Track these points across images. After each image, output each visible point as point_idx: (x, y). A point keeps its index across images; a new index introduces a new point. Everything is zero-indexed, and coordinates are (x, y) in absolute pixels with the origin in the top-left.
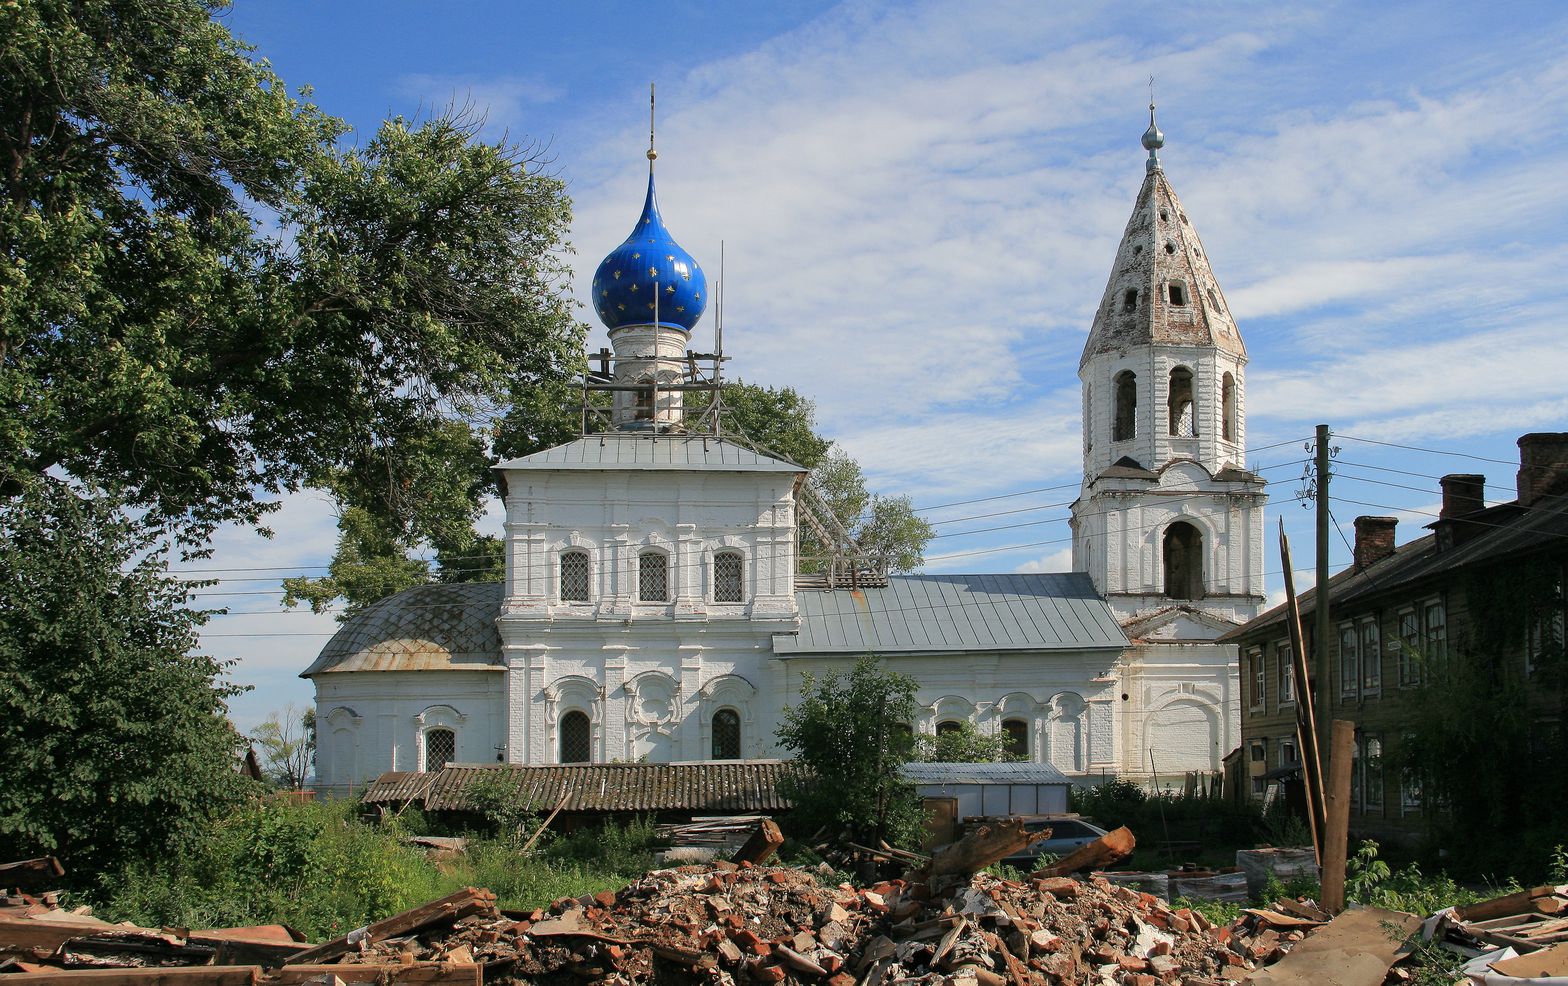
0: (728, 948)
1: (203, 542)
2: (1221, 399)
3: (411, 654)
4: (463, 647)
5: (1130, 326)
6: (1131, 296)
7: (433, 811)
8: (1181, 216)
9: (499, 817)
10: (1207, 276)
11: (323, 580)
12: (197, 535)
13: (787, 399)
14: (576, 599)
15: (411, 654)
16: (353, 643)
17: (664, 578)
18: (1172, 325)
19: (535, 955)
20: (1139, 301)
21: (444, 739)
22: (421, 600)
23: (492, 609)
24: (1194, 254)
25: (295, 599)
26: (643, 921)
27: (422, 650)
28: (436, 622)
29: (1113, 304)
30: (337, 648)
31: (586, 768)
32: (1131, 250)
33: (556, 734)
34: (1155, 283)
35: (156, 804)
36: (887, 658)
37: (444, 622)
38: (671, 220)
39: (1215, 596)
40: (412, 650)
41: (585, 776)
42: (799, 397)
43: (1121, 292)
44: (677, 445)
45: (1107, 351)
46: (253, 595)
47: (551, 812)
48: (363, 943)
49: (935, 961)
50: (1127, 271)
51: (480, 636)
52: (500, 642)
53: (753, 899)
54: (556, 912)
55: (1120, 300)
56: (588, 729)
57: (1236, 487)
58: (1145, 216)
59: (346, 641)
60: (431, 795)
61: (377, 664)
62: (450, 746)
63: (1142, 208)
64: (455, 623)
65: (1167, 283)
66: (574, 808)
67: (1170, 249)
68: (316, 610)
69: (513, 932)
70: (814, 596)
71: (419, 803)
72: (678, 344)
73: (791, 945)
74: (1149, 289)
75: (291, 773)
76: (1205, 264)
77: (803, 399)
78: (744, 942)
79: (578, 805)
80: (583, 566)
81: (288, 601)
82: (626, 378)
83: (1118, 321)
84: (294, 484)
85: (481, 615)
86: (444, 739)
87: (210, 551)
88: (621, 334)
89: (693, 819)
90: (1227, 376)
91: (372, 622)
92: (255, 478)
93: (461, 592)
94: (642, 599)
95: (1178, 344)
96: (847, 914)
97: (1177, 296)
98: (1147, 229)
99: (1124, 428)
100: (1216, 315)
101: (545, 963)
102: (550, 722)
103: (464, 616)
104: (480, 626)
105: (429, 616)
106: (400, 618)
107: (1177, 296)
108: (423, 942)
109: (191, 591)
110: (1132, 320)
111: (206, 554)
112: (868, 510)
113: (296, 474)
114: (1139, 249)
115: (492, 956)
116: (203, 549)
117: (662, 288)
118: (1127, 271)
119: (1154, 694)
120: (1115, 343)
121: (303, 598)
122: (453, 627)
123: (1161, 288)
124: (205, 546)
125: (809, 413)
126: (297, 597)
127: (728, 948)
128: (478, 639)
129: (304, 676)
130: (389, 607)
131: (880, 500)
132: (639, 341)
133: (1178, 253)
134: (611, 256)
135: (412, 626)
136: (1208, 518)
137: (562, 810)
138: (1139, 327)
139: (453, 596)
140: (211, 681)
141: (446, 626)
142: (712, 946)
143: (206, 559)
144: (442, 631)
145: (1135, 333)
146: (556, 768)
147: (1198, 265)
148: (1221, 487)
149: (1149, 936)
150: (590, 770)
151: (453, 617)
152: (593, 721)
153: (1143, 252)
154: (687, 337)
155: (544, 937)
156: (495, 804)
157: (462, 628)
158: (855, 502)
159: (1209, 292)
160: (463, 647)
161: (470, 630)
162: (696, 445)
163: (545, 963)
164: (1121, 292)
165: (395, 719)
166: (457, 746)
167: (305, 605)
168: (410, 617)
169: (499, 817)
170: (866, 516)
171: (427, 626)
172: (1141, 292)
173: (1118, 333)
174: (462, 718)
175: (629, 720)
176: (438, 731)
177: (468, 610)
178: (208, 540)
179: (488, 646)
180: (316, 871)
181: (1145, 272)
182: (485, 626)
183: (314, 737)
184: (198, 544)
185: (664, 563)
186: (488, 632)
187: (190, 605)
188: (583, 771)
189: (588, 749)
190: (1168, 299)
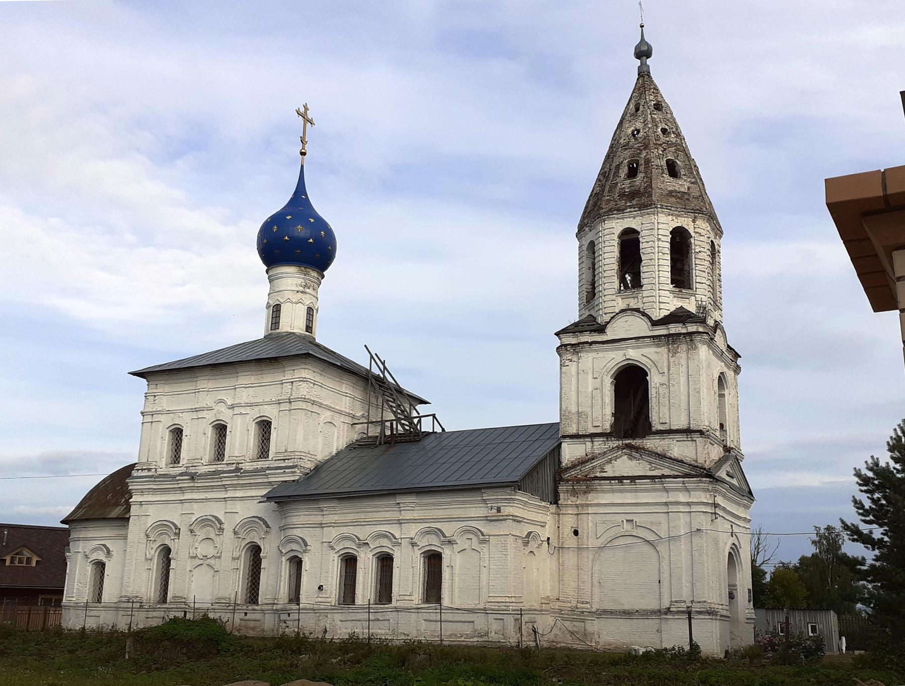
18: (622, 195)
148: (661, 331)
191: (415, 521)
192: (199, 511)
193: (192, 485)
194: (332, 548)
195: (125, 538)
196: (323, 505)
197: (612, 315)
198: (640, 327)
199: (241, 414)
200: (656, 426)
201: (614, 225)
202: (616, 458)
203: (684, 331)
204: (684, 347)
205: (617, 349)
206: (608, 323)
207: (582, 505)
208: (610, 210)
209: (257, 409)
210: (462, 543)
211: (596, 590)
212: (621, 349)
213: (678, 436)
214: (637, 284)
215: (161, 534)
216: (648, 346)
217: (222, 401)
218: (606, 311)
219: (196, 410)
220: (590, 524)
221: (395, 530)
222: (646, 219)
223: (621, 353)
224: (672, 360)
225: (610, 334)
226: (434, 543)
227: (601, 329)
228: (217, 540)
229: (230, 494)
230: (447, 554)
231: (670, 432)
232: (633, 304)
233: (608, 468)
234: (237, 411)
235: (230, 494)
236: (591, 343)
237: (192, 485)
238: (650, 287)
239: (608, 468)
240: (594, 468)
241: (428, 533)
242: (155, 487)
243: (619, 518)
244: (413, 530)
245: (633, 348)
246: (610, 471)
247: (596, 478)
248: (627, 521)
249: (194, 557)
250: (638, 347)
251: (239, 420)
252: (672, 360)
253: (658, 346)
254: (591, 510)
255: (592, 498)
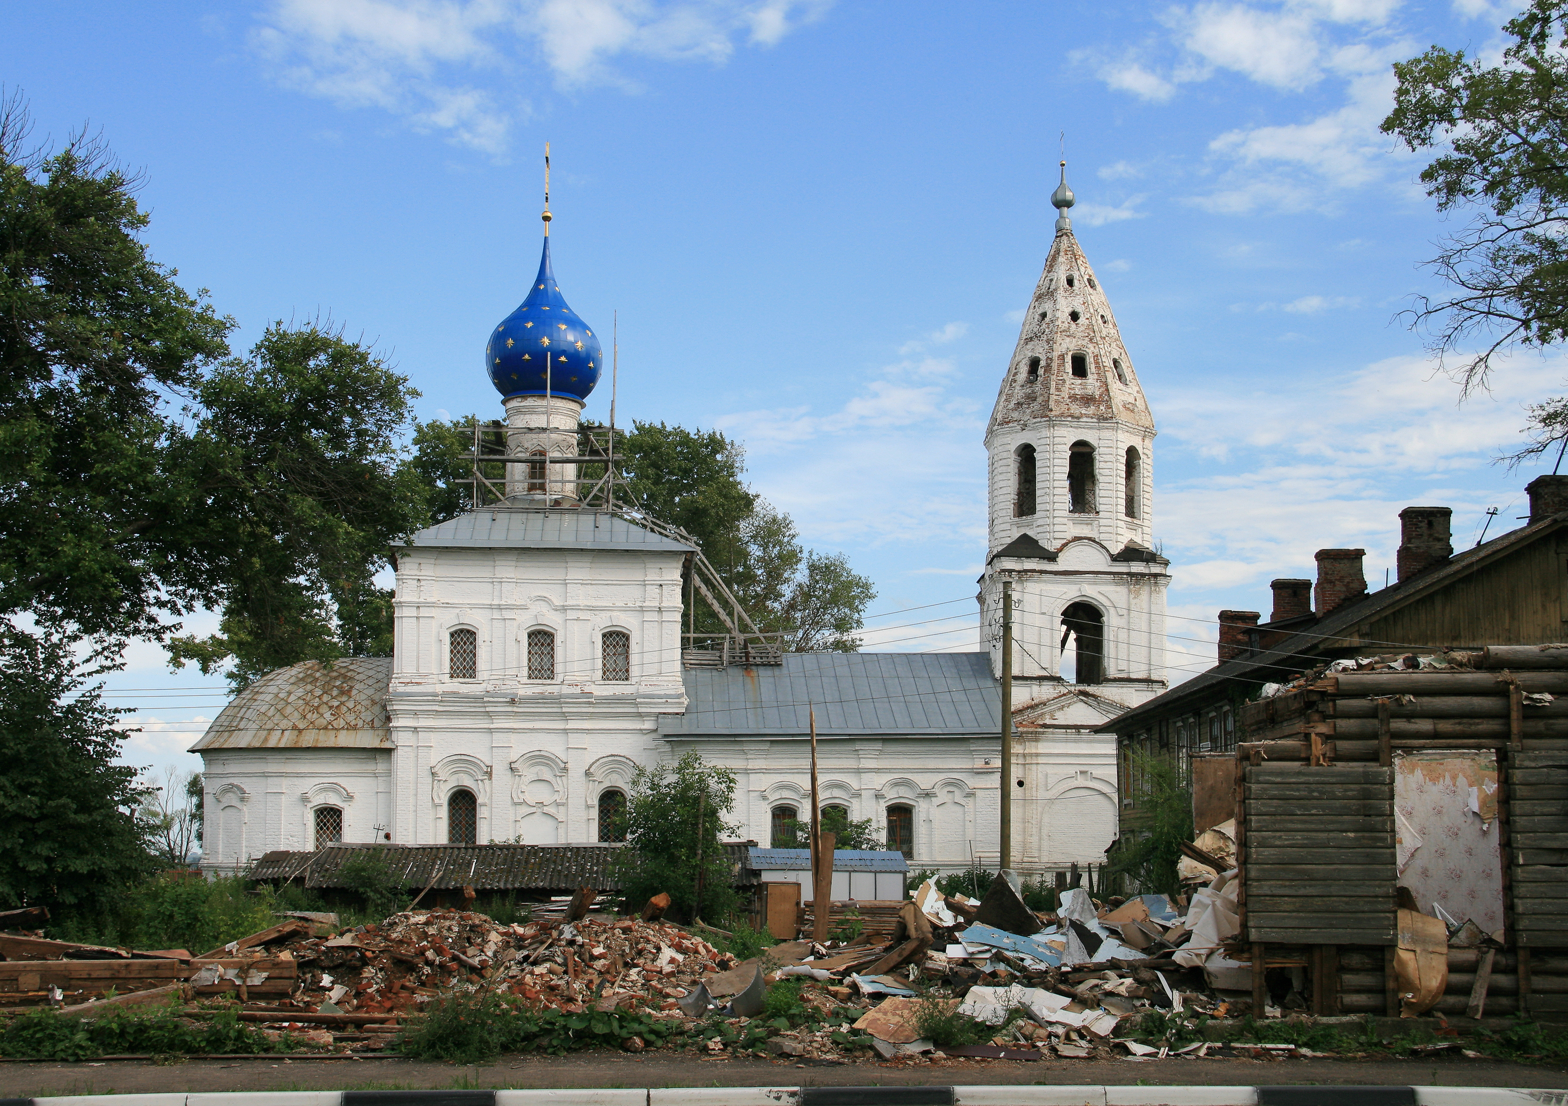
0: (430, 954)
1: (117, 657)
2: (1123, 475)
3: (300, 731)
4: (352, 724)
5: (1031, 398)
6: (1034, 364)
7: (313, 888)
8: (1089, 281)
9: (371, 894)
10: (1114, 345)
11: (213, 637)
12: (112, 652)
13: (716, 444)
14: (464, 676)
15: (300, 731)
16: (242, 718)
17: (552, 657)
18: (1073, 398)
19: (327, 957)
20: (1041, 371)
21: (332, 817)
22: (311, 675)
23: (380, 685)
24: (1100, 321)
25: (182, 659)
26: (386, 938)
27: (311, 726)
28: (325, 698)
29: (1016, 374)
30: (226, 724)
31: (459, 849)
32: (1037, 317)
33: (444, 812)
34: (1055, 354)
35: (91, 874)
36: (772, 742)
37: (333, 698)
38: (566, 285)
39: (1115, 680)
40: (301, 726)
41: (457, 856)
42: (727, 441)
43: (1024, 362)
44: (568, 520)
45: (1007, 423)
46: (156, 698)
47: (422, 890)
48: (234, 950)
49: (531, 959)
50: (1031, 339)
51: (369, 713)
52: (388, 719)
53: (450, 929)
54: (342, 934)
55: (1024, 369)
56: (475, 809)
57: (1137, 567)
58: (1051, 280)
59: (236, 716)
60: (311, 873)
61: (266, 740)
62: (338, 824)
63: (1049, 272)
64: (344, 699)
65: (1070, 354)
66: (443, 887)
67: (1075, 316)
68: (205, 670)
69: (317, 945)
70: (705, 676)
71: (299, 881)
72: (573, 413)
73: (464, 953)
74: (1051, 359)
75: (171, 850)
76: (1112, 331)
77: (732, 444)
78: (439, 951)
79: (448, 883)
80: (471, 643)
81: (176, 662)
82: (519, 449)
83: (1019, 393)
84: (192, 605)
85: (370, 692)
86: (332, 817)
87: (124, 665)
88: (514, 403)
89: (553, 898)
90: (1132, 453)
91: (261, 697)
92: (161, 604)
93: (351, 667)
94: (530, 677)
95: (1078, 418)
96: (500, 938)
97: (1079, 367)
98: (1052, 295)
99: (1026, 503)
100: (1121, 386)
101: (332, 961)
102: (437, 801)
103: (354, 692)
104: (369, 702)
105: (318, 692)
106: (290, 693)
107: (1079, 367)
108: (267, 950)
109: (117, 716)
110: (1033, 392)
111: (120, 667)
112: (802, 567)
113: (192, 597)
114: (1044, 315)
115: (304, 957)
116: (117, 663)
117: (555, 356)
118: (1031, 339)
119: (1051, 781)
120: (1015, 415)
121: (192, 657)
122: (342, 703)
123: (1062, 357)
124: (118, 660)
125: (738, 459)
126: (185, 657)
127: (430, 954)
128: (367, 716)
129: (193, 751)
130: (279, 682)
131: (815, 557)
132: (532, 411)
133: (1082, 320)
134: (504, 323)
135: (301, 702)
136: (1107, 595)
137: (432, 889)
138: (1040, 400)
139: (343, 671)
140: (130, 782)
141: (336, 703)
142: (422, 952)
143: (120, 671)
144: (331, 707)
145: (1036, 406)
146: (445, 848)
147: (1104, 334)
148: (1122, 568)
149: (668, 953)
150: (463, 850)
151: (342, 693)
152: (479, 801)
153: (1047, 320)
154: (583, 406)
155: (333, 947)
156: (369, 883)
157: (351, 705)
158: (790, 558)
159: (1115, 362)
160: (352, 724)
161: (359, 707)
162: (587, 520)
163: (332, 961)
164: (1024, 362)
165: (283, 796)
166: (345, 825)
167: (192, 665)
168: (300, 692)
169: (371, 894)
170: (801, 575)
171: (316, 702)
172: (1043, 363)
173: (1019, 404)
174: (350, 797)
175: (516, 800)
176: (325, 809)
177: (357, 687)
178: (121, 656)
179: (377, 723)
180: (207, 927)
181: (1048, 341)
182: (374, 703)
183: (200, 806)
184: (113, 660)
185: (553, 641)
186: (377, 709)
187: (117, 727)
188: (456, 852)
189: (475, 829)
190: (1070, 371)
191: (877, 771)
192: (520, 747)
193: (510, 709)
194: (765, 798)
195: (389, 773)
196: (746, 747)
197: (1065, 541)
198: (1098, 561)
199: (578, 619)
200: (1112, 672)
201: (1065, 433)
202: (1069, 705)
203: (1146, 571)
204: (1146, 589)
205: (1070, 583)
206: (1060, 550)
207: (1031, 755)
208: (1062, 415)
209: (605, 615)
210: (942, 795)
211: (1045, 844)
212: (1075, 583)
213: (1137, 685)
214: (1032, 510)
215: (455, 772)
216: (1106, 584)
217: (544, 599)
218: (1057, 535)
219: (500, 608)
220: (1040, 775)
221: (853, 781)
222: (1106, 434)
223: (1075, 588)
224: (1133, 602)
225: (1062, 564)
226: (904, 796)
227: (1052, 557)
228: (558, 784)
229: (572, 725)
230: (922, 812)
231: (1130, 680)
232: (1085, 531)
233: (1058, 715)
234: (571, 614)
235: (572, 725)
236: (1042, 572)
237: (510, 709)
238: (1107, 515)
239: (1058, 715)
240: (1043, 714)
241: (896, 784)
242: (441, 709)
243: (1071, 770)
244: (879, 781)
245: (1090, 584)
246: (1062, 718)
247: (1045, 726)
248: (1081, 772)
249: (520, 804)
250: (1095, 584)
251: (575, 627)
252: (1133, 602)
253: (1117, 584)
254: (1040, 760)
255: (1042, 747)
